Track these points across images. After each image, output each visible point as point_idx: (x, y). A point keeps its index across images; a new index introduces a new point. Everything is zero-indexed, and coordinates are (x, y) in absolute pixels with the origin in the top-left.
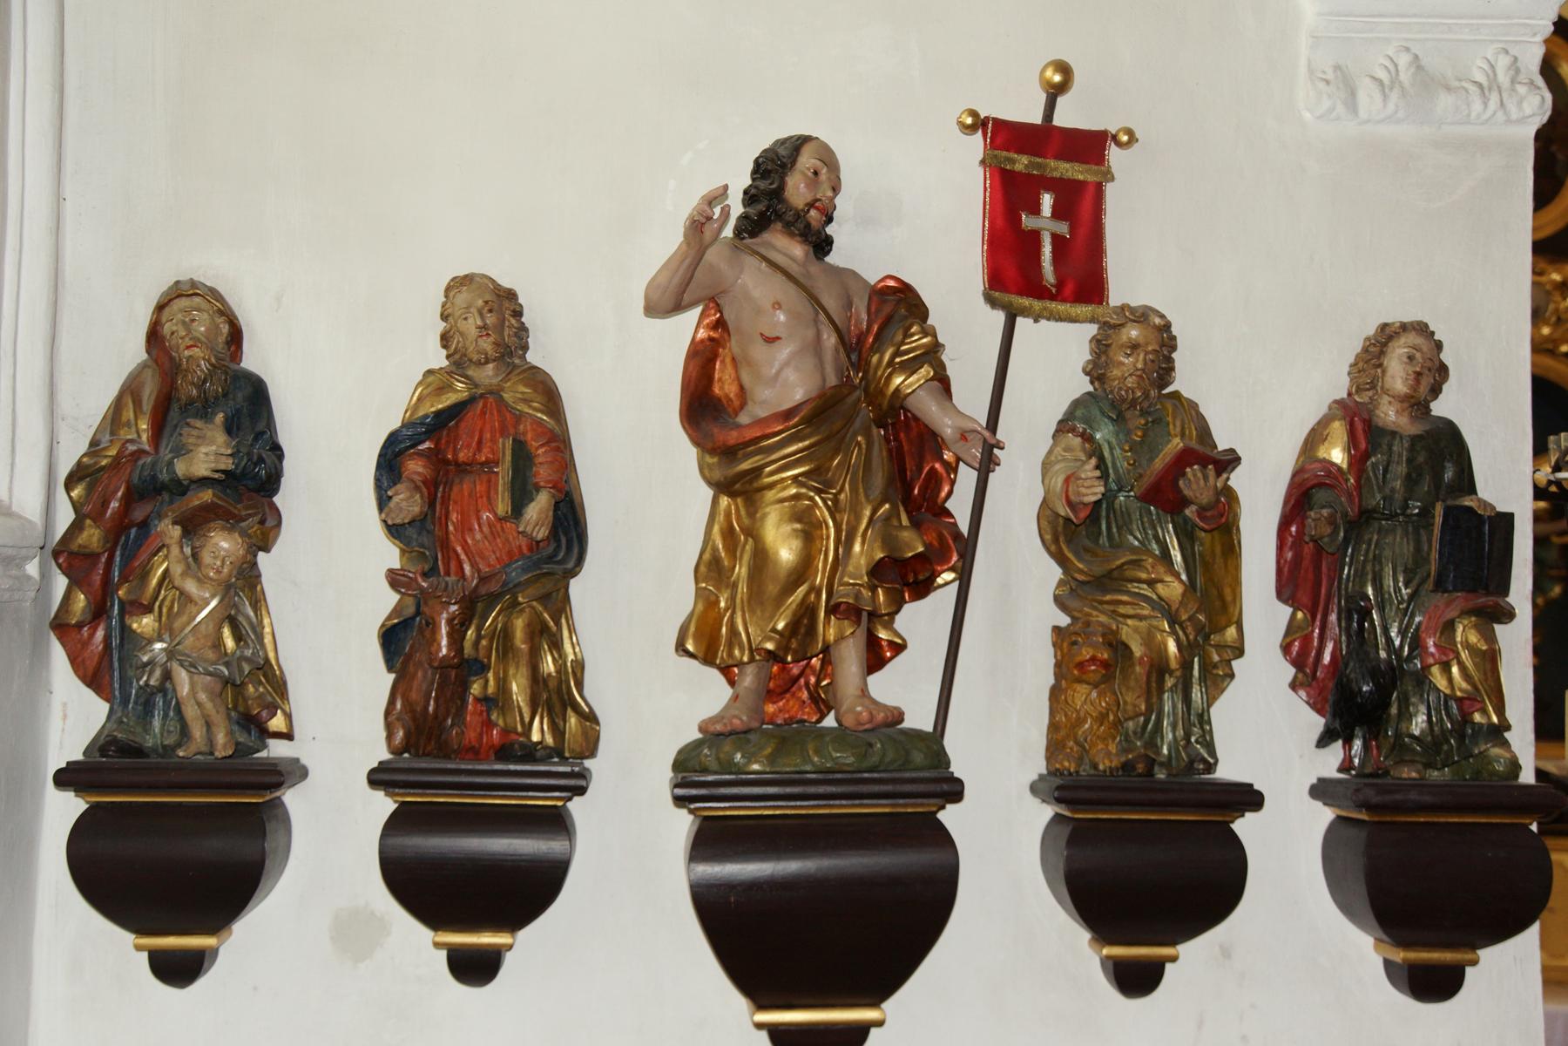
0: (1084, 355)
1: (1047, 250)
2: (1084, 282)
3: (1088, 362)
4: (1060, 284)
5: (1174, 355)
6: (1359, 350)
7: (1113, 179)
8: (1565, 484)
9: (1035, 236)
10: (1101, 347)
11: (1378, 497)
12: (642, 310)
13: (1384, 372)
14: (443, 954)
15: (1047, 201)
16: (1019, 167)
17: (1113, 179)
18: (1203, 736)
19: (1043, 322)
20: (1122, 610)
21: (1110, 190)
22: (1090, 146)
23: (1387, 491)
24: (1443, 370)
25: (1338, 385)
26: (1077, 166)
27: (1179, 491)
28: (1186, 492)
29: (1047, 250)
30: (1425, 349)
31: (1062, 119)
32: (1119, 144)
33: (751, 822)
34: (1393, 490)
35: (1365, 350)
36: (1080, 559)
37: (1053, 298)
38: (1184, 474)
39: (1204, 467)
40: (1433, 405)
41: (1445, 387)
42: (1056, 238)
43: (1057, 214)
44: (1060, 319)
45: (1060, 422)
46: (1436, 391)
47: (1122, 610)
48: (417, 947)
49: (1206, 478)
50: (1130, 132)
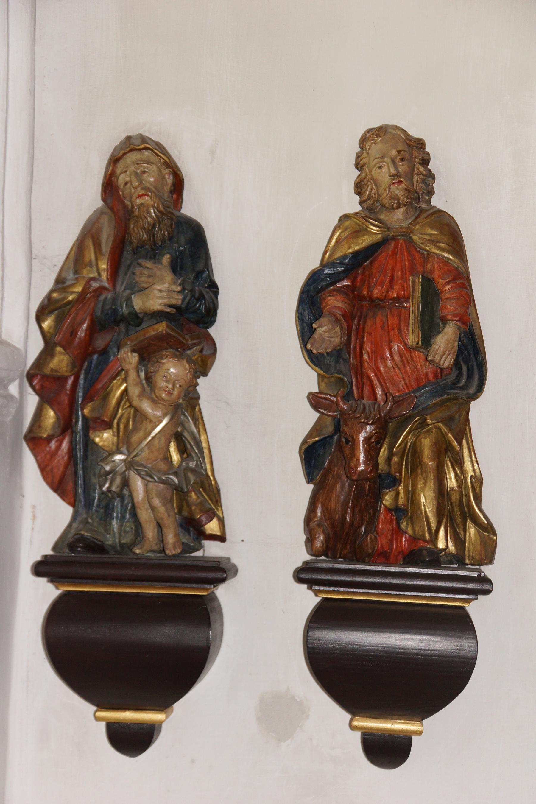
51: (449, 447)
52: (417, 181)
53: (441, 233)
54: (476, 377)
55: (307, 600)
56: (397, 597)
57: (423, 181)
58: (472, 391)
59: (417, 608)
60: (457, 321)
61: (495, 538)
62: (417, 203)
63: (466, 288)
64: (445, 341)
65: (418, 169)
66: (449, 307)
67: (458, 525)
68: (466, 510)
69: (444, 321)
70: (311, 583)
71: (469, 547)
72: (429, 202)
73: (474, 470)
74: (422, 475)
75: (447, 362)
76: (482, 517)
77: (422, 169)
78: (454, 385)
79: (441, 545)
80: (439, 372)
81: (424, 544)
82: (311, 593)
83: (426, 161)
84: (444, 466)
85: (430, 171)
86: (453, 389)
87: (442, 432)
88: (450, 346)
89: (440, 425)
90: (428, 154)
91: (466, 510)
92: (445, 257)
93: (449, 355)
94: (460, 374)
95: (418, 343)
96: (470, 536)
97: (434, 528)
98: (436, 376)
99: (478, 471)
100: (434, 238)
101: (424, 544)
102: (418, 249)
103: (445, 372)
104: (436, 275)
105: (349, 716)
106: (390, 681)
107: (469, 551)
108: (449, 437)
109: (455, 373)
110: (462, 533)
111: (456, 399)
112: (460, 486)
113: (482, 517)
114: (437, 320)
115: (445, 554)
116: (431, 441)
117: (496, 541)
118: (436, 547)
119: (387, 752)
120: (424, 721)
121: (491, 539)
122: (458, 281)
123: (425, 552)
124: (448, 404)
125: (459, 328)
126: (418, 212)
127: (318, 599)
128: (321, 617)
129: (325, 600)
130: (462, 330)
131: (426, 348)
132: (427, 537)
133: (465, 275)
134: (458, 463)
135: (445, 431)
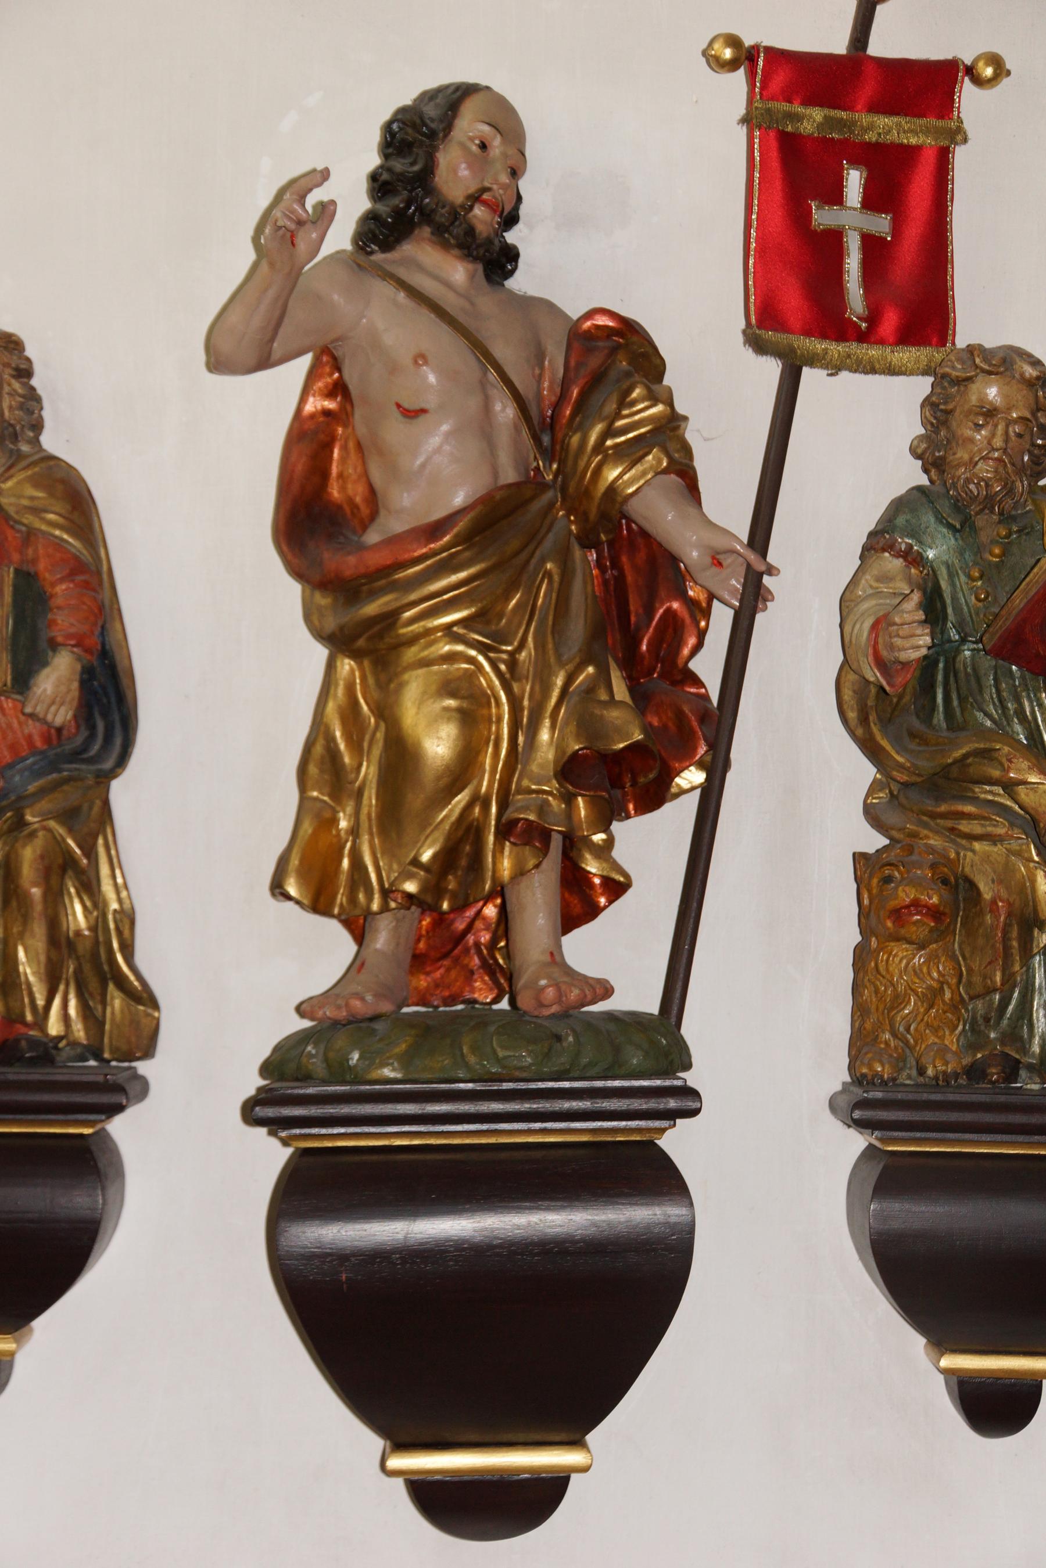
0: (912, 426)
1: (853, 263)
3: (920, 438)
4: (873, 317)
7: (965, 140)
15: (854, 181)
16: (807, 128)
19: (845, 375)
20: (964, 826)
21: (961, 156)
22: (929, 87)
29: (853, 263)
31: (879, 47)
32: (978, 81)
37: (863, 337)
42: (870, 243)
43: (871, 202)
45: (872, 535)
47: (964, 826)
50: (996, 61)
51: (68, 863)
52: (10, 407)
53: (52, 495)
54: (118, 741)
55: (269, 1156)
56: (407, 1137)
57: (21, 407)
58: (108, 765)
60: (73, 646)
61: (156, 1014)
62: (12, 443)
63: (94, 590)
64: (56, 682)
65: (9, 385)
66: (65, 619)
67: (91, 995)
68: (106, 968)
69: (54, 646)
70: (861, 1125)
71: (111, 1032)
72: (36, 442)
73: (120, 900)
74: (19, 910)
75: (62, 715)
76: (132, 978)
77: (16, 385)
78: (77, 755)
79: (54, 1027)
80: (55, 734)
81: (23, 1030)
83: (25, 372)
84: (62, 895)
85: (33, 389)
86: (71, 762)
87: (55, 838)
88: (63, 689)
89: (52, 824)
90: (28, 360)
91: (106, 968)
92: (56, 537)
93: (62, 704)
94: (92, 736)
95: (5, 685)
96: (113, 1013)
97: (40, 1002)
98: (47, 739)
99: (127, 902)
100: (36, 503)
101: (23, 1030)
102: (11, 523)
103: (65, 732)
104: (41, 566)
107: (111, 1038)
108: (68, 845)
109: (84, 733)
110: (99, 1007)
111: (82, 779)
112: (93, 929)
113: (132, 978)
114: (43, 644)
115: (68, 1045)
116: (34, 851)
117: (158, 1020)
118: (47, 1035)
120: (591, 1438)
121: (148, 1015)
122: (79, 578)
123: (23, 1043)
124: (65, 788)
125: (79, 659)
126: (14, 458)
127: (289, 1151)
130: (85, 662)
131: (21, 693)
132: (29, 1017)
133: (93, 568)
134: (90, 887)
135: (61, 835)
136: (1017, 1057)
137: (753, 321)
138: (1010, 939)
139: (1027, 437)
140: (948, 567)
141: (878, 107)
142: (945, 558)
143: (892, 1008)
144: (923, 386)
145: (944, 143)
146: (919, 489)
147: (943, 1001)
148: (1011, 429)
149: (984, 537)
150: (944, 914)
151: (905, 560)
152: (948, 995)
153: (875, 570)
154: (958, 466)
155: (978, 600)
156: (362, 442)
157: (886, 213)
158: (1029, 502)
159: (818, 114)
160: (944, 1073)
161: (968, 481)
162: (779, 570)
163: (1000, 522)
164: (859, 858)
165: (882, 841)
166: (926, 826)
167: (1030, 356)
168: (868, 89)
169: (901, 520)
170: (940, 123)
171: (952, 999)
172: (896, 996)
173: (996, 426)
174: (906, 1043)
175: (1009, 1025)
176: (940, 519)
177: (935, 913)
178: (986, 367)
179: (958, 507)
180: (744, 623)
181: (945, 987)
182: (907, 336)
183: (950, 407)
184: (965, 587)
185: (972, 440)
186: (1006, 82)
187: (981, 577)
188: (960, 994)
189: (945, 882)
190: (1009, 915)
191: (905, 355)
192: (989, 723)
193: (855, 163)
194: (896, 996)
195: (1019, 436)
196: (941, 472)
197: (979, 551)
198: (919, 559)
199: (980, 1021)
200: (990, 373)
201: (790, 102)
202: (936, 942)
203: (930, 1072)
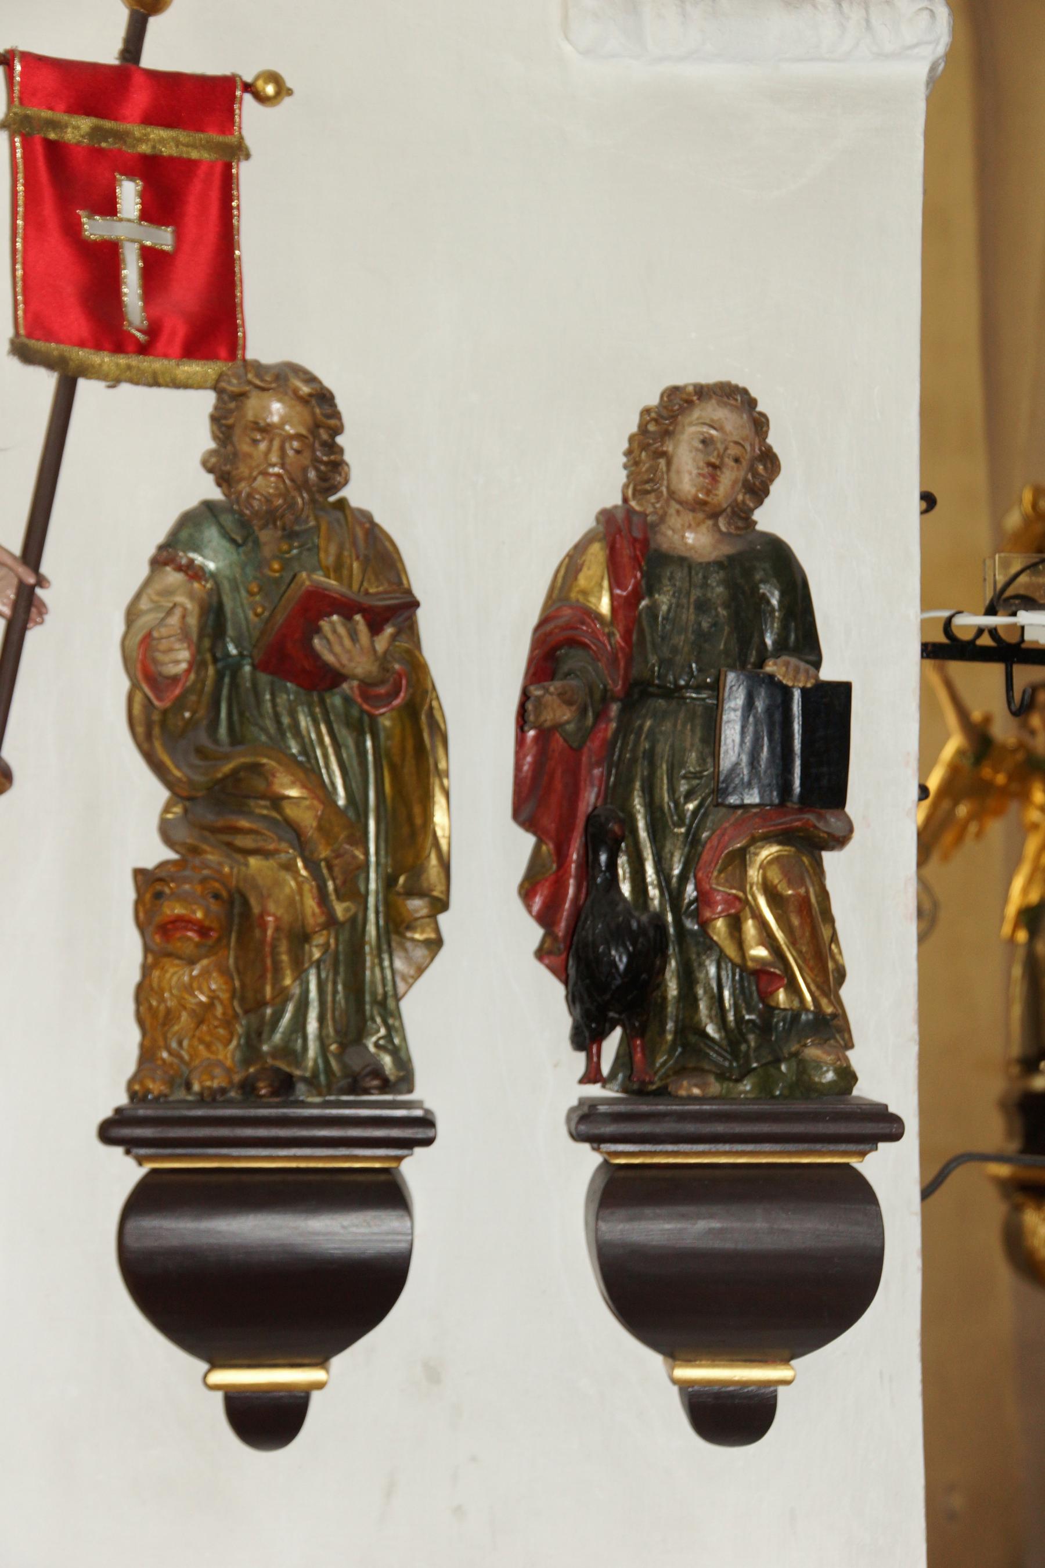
0: (205, 441)
1: (131, 273)
2: (212, 327)
3: (212, 453)
4: (153, 330)
5: (340, 440)
6: (634, 429)
7: (248, 156)
8: (1001, 633)
9: (108, 254)
10: (223, 424)
11: (653, 659)
12: (6, 346)
13: (669, 464)
14: (219, 1397)
15: (129, 194)
16: (70, 136)
17: (248, 156)
18: (389, 1037)
19: (125, 388)
20: (241, 841)
21: (245, 172)
22: (207, 102)
23: (666, 653)
24: (769, 461)
25: (606, 484)
26: (182, 136)
27: (316, 657)
28: (329, 658)
29: (131, 273)
30: (729, 427)
31: (155, 56)
32: (261, 98)
33: (318, 1177)
34: (675, 650)
35: (643, 429)
36: (178, 767)
37: (143, 350)
38: (318, 630)
39: (348, 617)
40: (758, 515)
41: (774, 488)
42: (151, 257)
43: (150, 214)
44: (186, 386)
45: (161, 548)
46: (759, 492)
47: (241, 841)
48: (184, 1387)
49: (354, 636)
50: (274, 78)
55: (124, 1172)
59: (258, 1178)
70: (130, 1145)
82: (130, 1162)
105: (203, 1366)
106: (720, 1290)
119: (266, 1421)
128: (144, 1200)
129: (154, 1171)
136: (287, 1069)
137: (22, 331)
138: (279, 954)
139: (307, 454)
140: (229, 581)
141: (150, 119)
142: (228, 572)
143: (164, 1024)
144: (206, 401)
145: (227, 159)
146: (209, 507)
147: (216, 1018)
148: (287, 445)
149: (267, 552)
150: (210, 929)
151: (187, 574)
152: (219, 1010)
153: (157, 586)
154: (241, 480)
155: (257, 615)
156: (1029, 563)
157: (167, 225)
158: (311, 518)
159: (85, 124)
160: (210, 1088)
161: (250, 496)
162: (48, 582)
163: (283, 537)
164: (139, 874)
165: (171, 855)
166: (204, 840)
167: (306, 372)
168: (140, 98)
169: (184, 535)
170: (221, 138)
171: (224, 1014)
172: (168, 1011)
173: (271, 441)
174: (180, 1058)
175: (282, 1039)
176: (225, 534)
177: (203, 931)
178: (258, 382)
179: (244, 524)
180: (15, 637)
181: (217, 1002)
182: (192, 350)
183: (230, 421)
184: (245, 602)
185: (250, 456)
186: (287, 101)
187: (261, 589)
188: (234, 1010)
189: (217, 896)
190: (277, 929)
191: (193, 368)
192: (263, 738)
193: (130, 174)
194: (168, 1011)
195: (298, 452)
196: (230, 486)
197: (260, 565)
198: (201, 573)
199: (253, 1036)
200: (263, 389)
201: (51, 108)
202: (206, 956)
203: (196, 1087)
